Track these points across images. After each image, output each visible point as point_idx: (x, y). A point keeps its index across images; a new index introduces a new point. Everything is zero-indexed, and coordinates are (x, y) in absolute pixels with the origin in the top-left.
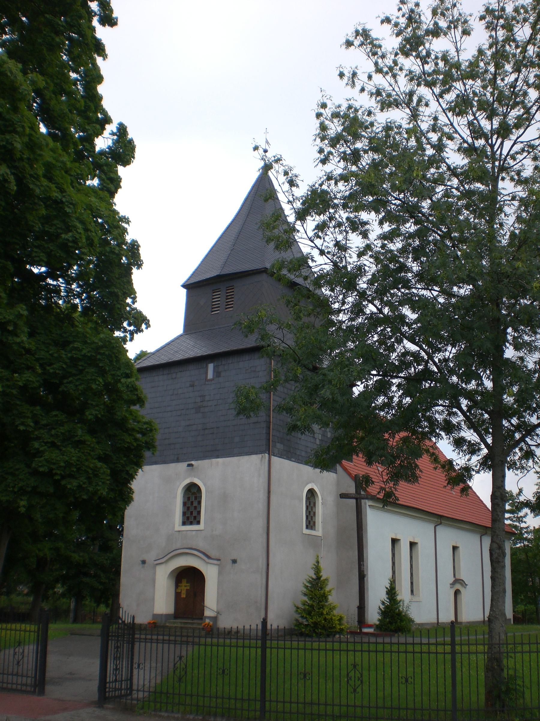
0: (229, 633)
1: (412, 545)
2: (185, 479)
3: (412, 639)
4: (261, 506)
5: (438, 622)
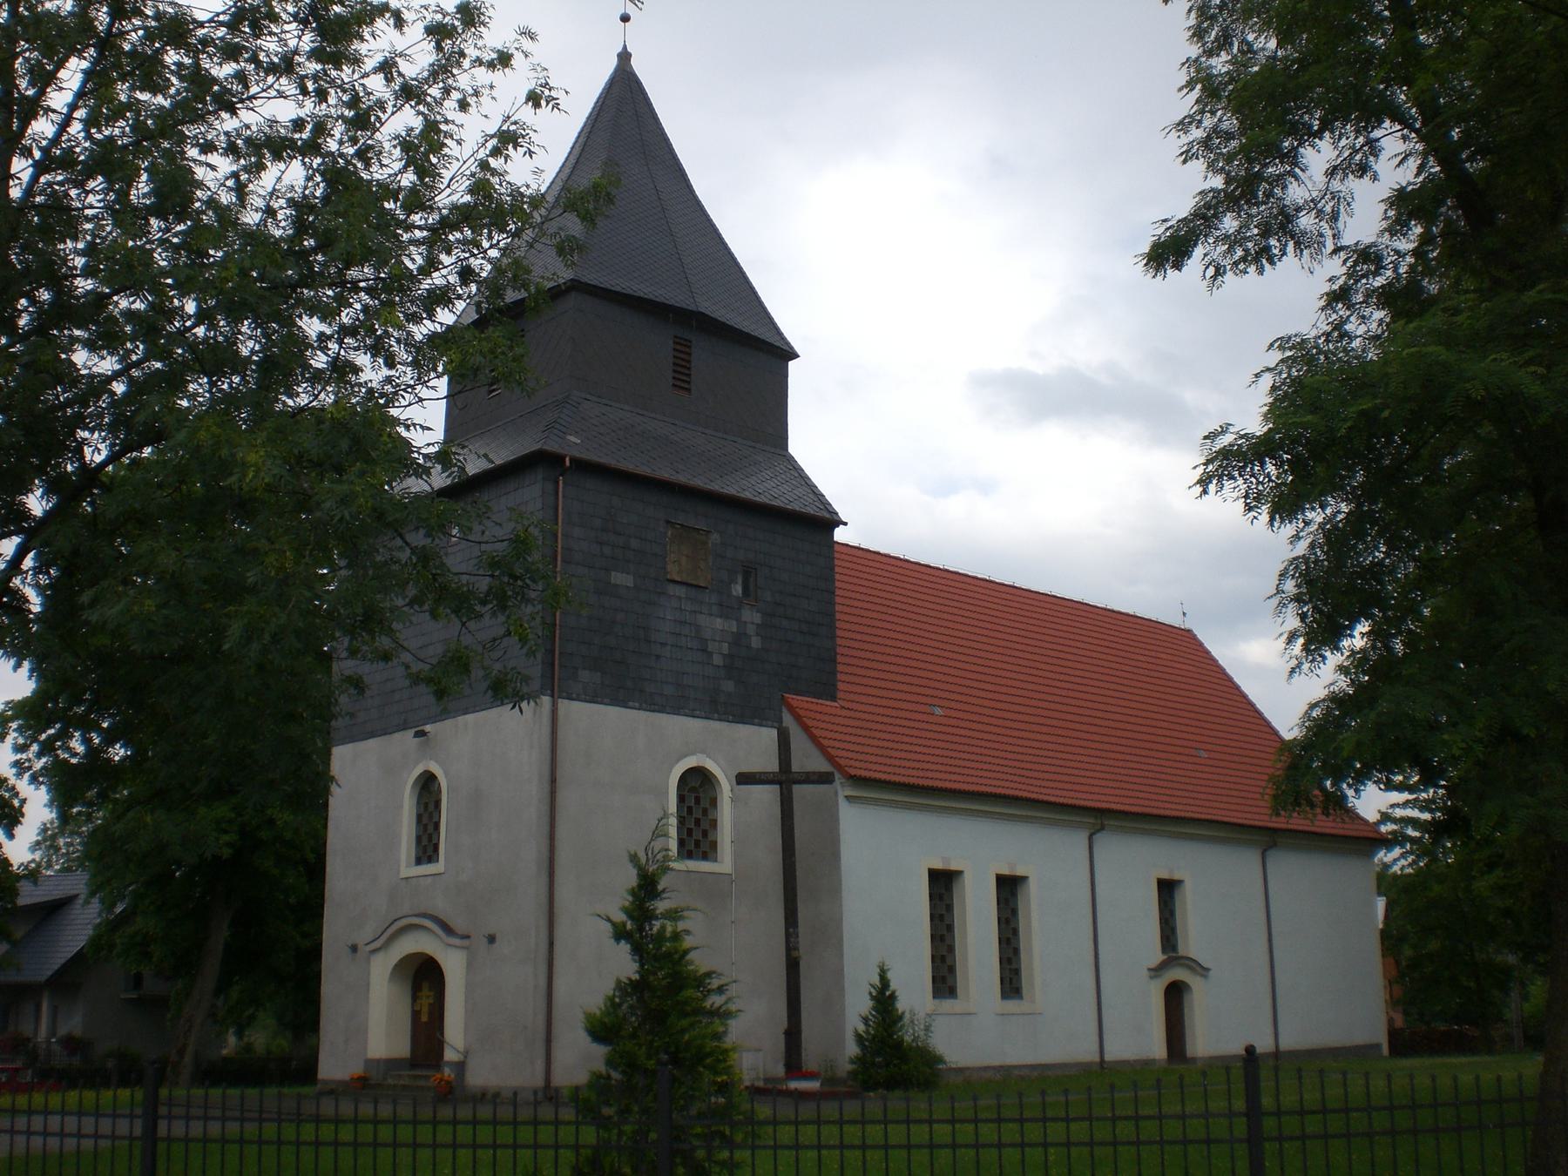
0: (483, 1097)
1: (1009, 887)
2: (417, 763)
3: (371, 1106)
4: (533, 812)
5: (1102, 1060)
